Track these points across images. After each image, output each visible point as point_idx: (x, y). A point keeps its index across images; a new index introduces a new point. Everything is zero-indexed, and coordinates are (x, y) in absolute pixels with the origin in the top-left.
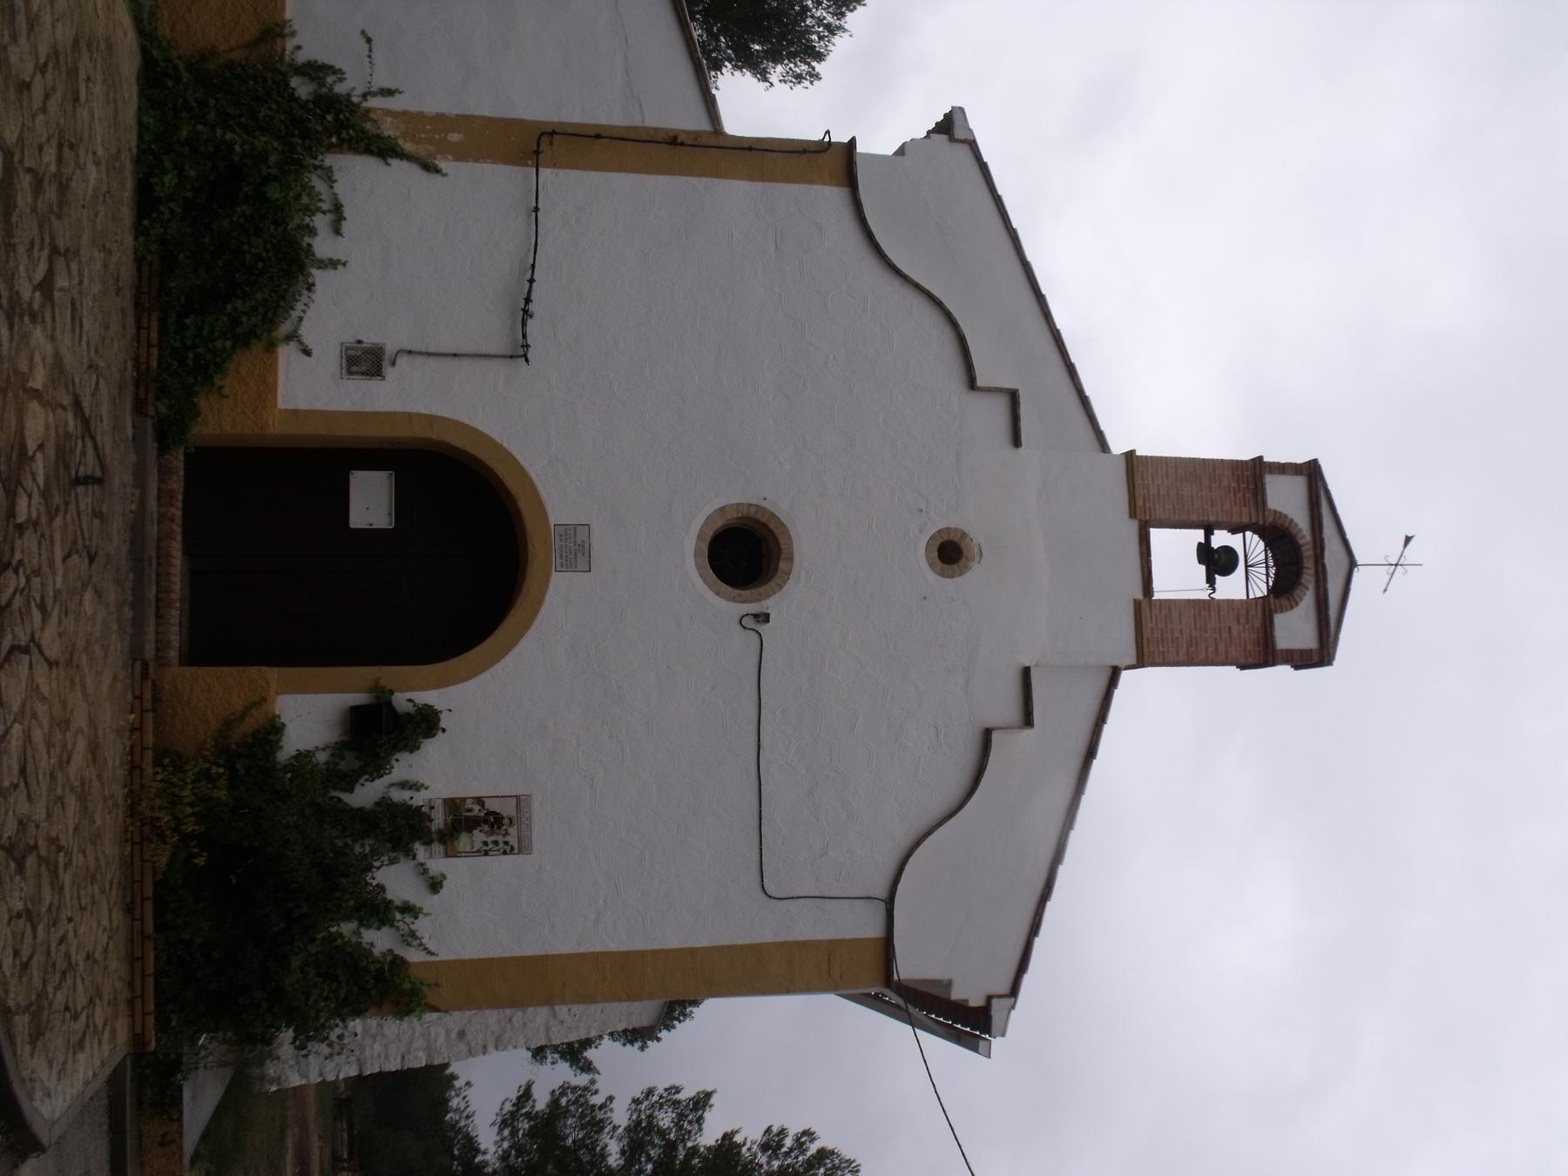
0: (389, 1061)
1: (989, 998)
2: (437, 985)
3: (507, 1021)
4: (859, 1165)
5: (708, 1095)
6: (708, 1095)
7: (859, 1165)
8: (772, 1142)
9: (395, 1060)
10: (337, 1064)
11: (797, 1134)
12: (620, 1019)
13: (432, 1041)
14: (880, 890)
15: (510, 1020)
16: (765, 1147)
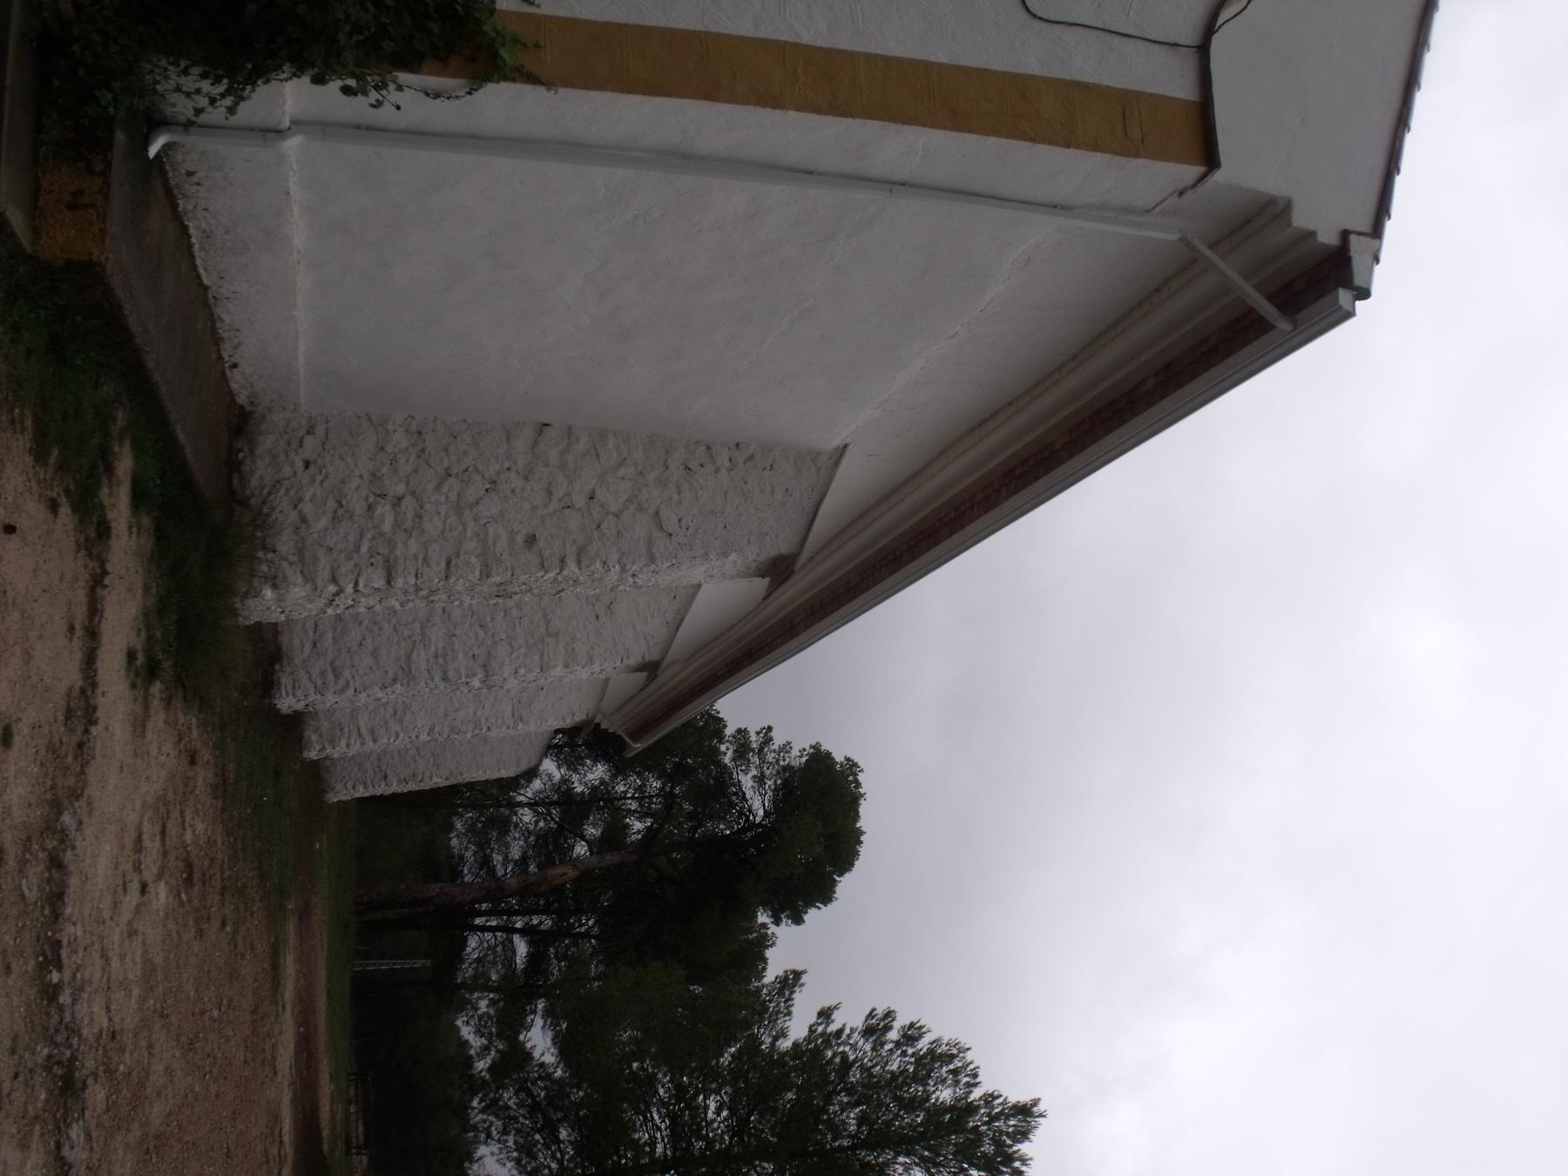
0: (428, 566)
1: (1345, 234)
2: (537, 46)
3: (594, 526)
4: (978, 1068)
5: (797, 975)
6: (797, 975)
7: (978, 1068)
8: (876, 1028)
9: (438, 564)
10: (356, 565)
11: (903, 1028)
12: (749, 540)
13: (490, 543)
14: (1188, 33)
15: (599, 526)
16: (869, 1031)
